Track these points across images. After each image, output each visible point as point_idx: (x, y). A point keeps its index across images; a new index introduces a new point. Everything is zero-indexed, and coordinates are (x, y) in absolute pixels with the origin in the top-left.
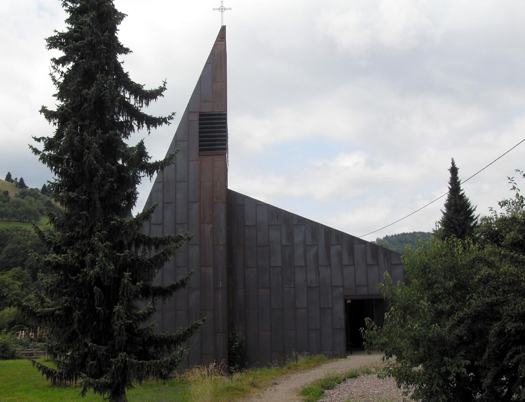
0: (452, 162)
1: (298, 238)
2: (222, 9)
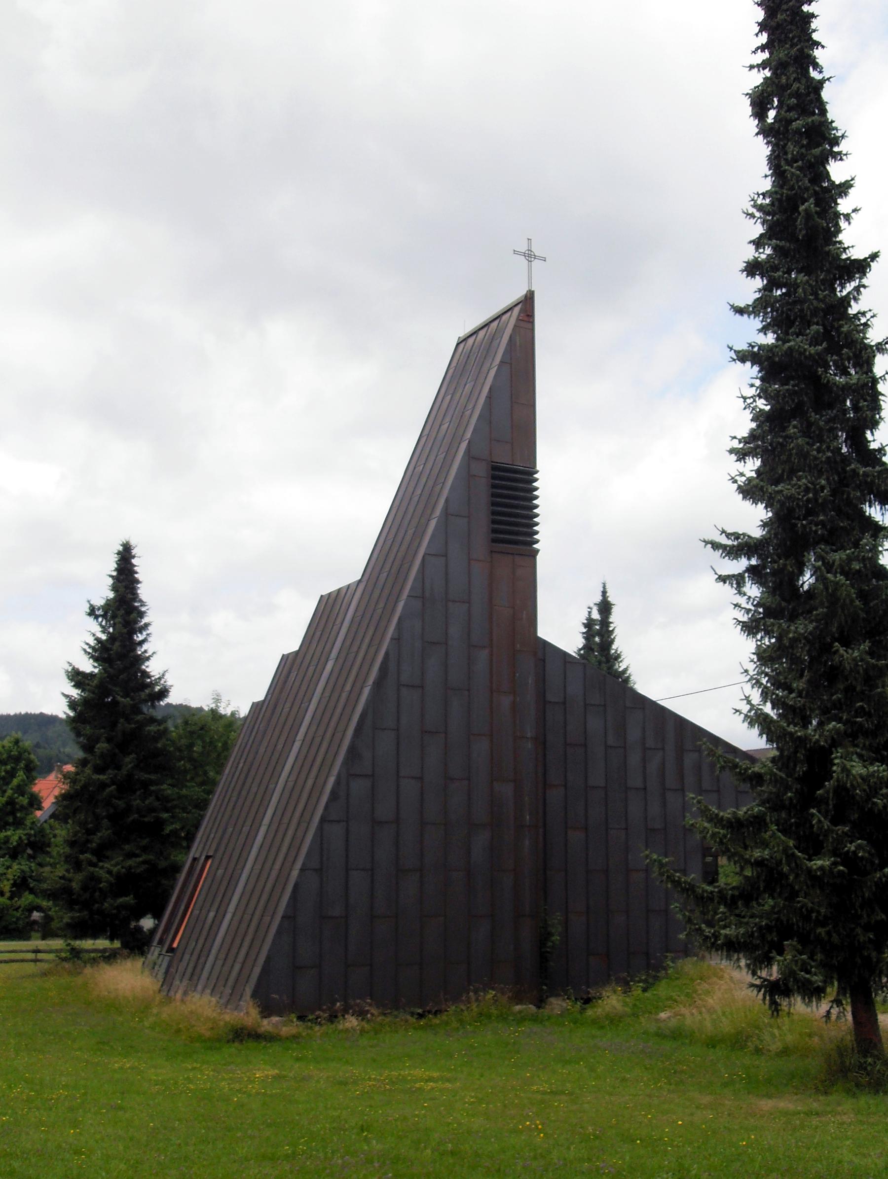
0: (602, 589)
1: (634, 734)
2: (529, 256)
